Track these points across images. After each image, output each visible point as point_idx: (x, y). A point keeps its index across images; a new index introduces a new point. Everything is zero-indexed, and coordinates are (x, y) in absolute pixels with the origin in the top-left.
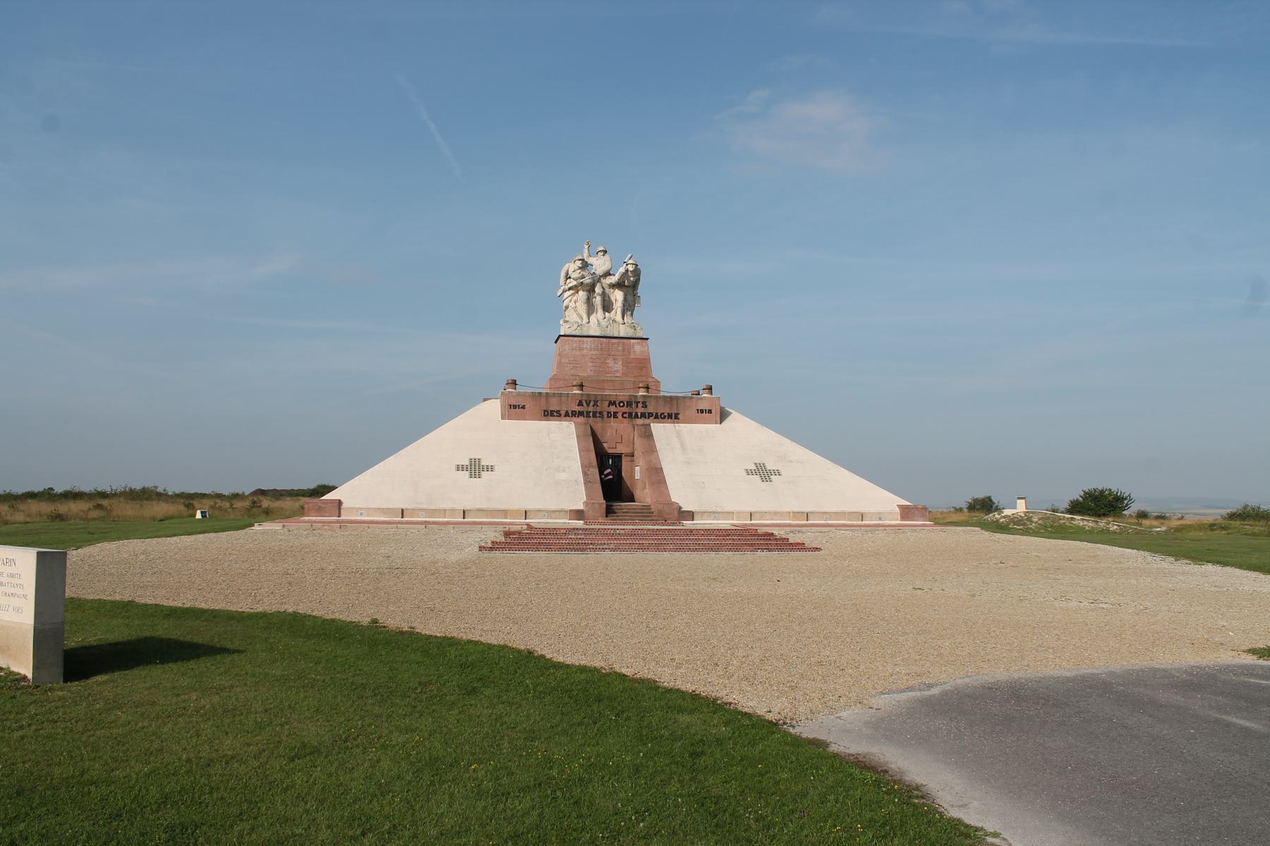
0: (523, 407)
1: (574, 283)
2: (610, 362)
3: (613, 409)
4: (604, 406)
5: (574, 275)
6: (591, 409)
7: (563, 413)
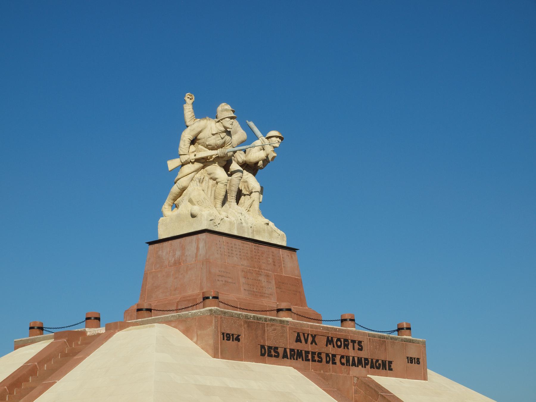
0: (238, 339)
1: (206, 153)
2: (263, 279)
3: (331, 350)
4: (321, 347)
5: (213, 141)
6: (309, 347)
7: (281, 351)
